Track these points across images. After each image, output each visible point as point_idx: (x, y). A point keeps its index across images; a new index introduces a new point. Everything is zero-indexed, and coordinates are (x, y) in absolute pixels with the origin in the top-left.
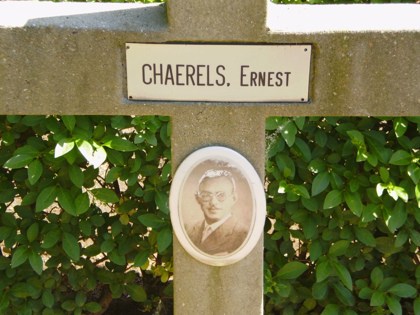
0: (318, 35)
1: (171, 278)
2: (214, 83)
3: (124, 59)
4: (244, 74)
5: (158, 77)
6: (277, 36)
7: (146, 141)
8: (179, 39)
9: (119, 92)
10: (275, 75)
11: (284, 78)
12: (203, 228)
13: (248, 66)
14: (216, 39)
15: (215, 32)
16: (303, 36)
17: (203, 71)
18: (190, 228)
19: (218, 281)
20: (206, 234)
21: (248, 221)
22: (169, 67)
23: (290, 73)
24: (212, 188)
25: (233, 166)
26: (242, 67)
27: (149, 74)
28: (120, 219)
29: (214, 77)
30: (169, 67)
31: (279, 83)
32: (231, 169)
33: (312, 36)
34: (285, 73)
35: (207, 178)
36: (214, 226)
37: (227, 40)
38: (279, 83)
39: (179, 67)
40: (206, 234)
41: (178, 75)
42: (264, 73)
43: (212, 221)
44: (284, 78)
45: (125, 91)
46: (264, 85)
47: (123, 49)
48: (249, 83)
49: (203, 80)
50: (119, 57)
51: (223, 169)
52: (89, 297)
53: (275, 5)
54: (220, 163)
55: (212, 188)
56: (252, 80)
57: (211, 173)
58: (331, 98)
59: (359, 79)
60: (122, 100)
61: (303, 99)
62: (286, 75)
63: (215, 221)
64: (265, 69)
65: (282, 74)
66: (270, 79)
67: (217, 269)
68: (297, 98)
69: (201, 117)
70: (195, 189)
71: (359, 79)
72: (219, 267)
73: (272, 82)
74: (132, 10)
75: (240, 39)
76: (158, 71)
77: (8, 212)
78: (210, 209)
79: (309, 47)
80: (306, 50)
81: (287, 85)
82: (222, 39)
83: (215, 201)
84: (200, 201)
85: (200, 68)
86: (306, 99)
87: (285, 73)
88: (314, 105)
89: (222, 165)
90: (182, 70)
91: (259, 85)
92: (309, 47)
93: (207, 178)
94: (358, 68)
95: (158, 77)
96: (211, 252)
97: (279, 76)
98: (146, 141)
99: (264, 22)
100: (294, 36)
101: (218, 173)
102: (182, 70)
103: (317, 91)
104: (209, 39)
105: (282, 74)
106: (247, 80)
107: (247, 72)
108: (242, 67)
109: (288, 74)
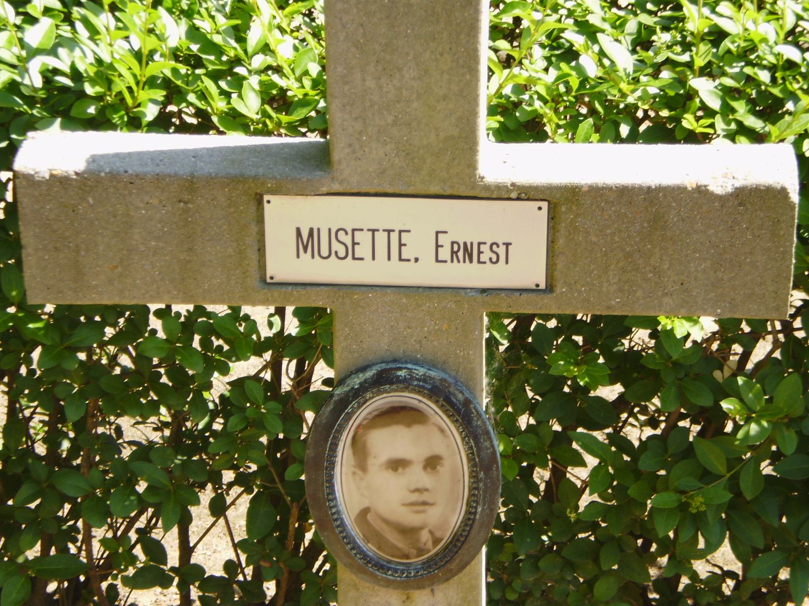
2: (488, 261)
4: (356, 241)
10: (488, 246)
11: (502, 251)
13: (446, 232)
16: (536, 188)
23: (510, 244)
26: (437, 233)
28: (227, 513)
31: (494, 260)
34: (504, 244)
38: (494, 260)
39: (439, 234)
42: (472, 244)
45: (536, 290)
46: (471, 261)
47: (259, 202)
48: (449, 259)
53: (498, 144)
61: (537, 285)
62: (505, 246)
65: (498, 246)
66: (480, 252)
68: (530, 284)
73: (484, 258)
74: (267, 147)
77: (271, 583)
79: (544, 205)
80: (540, 208)
81: (507, 262)
85: (356, 233)
86: (543, 286)
87: (504, 244)
91: (464, 261)
92: (544, 205)
97: (494, 247)
99: (475, 168)
105: (498, 246)
106: (445, 253)
107: (444, 240)
108: (437, 233)
109: (507, 245)
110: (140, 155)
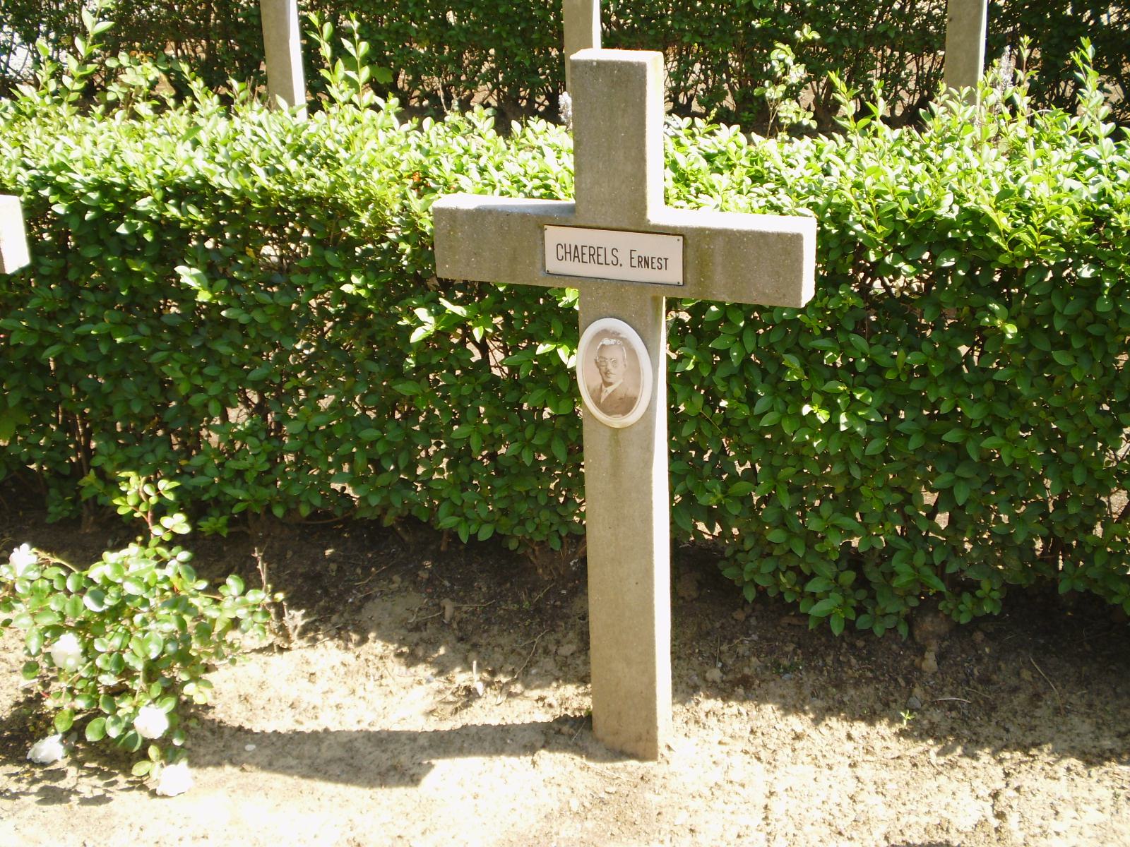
0: (686, 228)
1: (993, 723)
3: (543, 239)
5: (568, 255)
6: (655, 226)
7: (433, 247)
8: (582, 224)
9: (539, 265)
11: (663, 262)
12: (601, 390)
14: (609, 226)
15: (609, 220)
17: (601, 252)
18: (591, 389)
19: (617, 442)
20: (604, 396)
21: (638, 385)
22: (576, 247)
24: (608, 355)
25: (625, 336)
27: (561, 252)
29: (610, 258)
30: (576, 247)
32: (622, 339)
33: (681, 228)
35: (603, 345)
36: (610, 389)
37: (619, 227)
40: (604, 396)
41: (583, 254)
43: (608, 384)
44: (663, 262)
45: (544, 265)
47: (542, 230)
49: (602, 260)
50: (540, 237)
51: (616, 338)
52: (196, 193)
54: (614, 333)
55: (608, 355)
56: (639, 262)
57: (606, 341)
58: (699, 283)
59: (719, 269)
60: (541, 274)
63: (611, 384)
64: (649, 254)
67: (616, 431)
69: (600, 291)
70: (594, 355)
71: (719, 269)
72: (617, 429)
75: (628, 227)
76: (568, 251)
78: (606, 373)
79: (681, 238)
82: (614, 226)
83: (610, 367)
84: (598, 365)
88: (687, 288)
89: (615, 335)
90: (586, 250)
92: (681, 238)
93: (603, 345)
94: (719, 259)
95: (568, 255)
96: (608, 413)
98: (433, 247)
99: (645, 214)
100: (668, 228)
101: (612, 341)
102: (586, 250)
103: (688, 276)
104: (604, 225)
106: (635, 262)
107: (634, 254)
110: (528, 207)
